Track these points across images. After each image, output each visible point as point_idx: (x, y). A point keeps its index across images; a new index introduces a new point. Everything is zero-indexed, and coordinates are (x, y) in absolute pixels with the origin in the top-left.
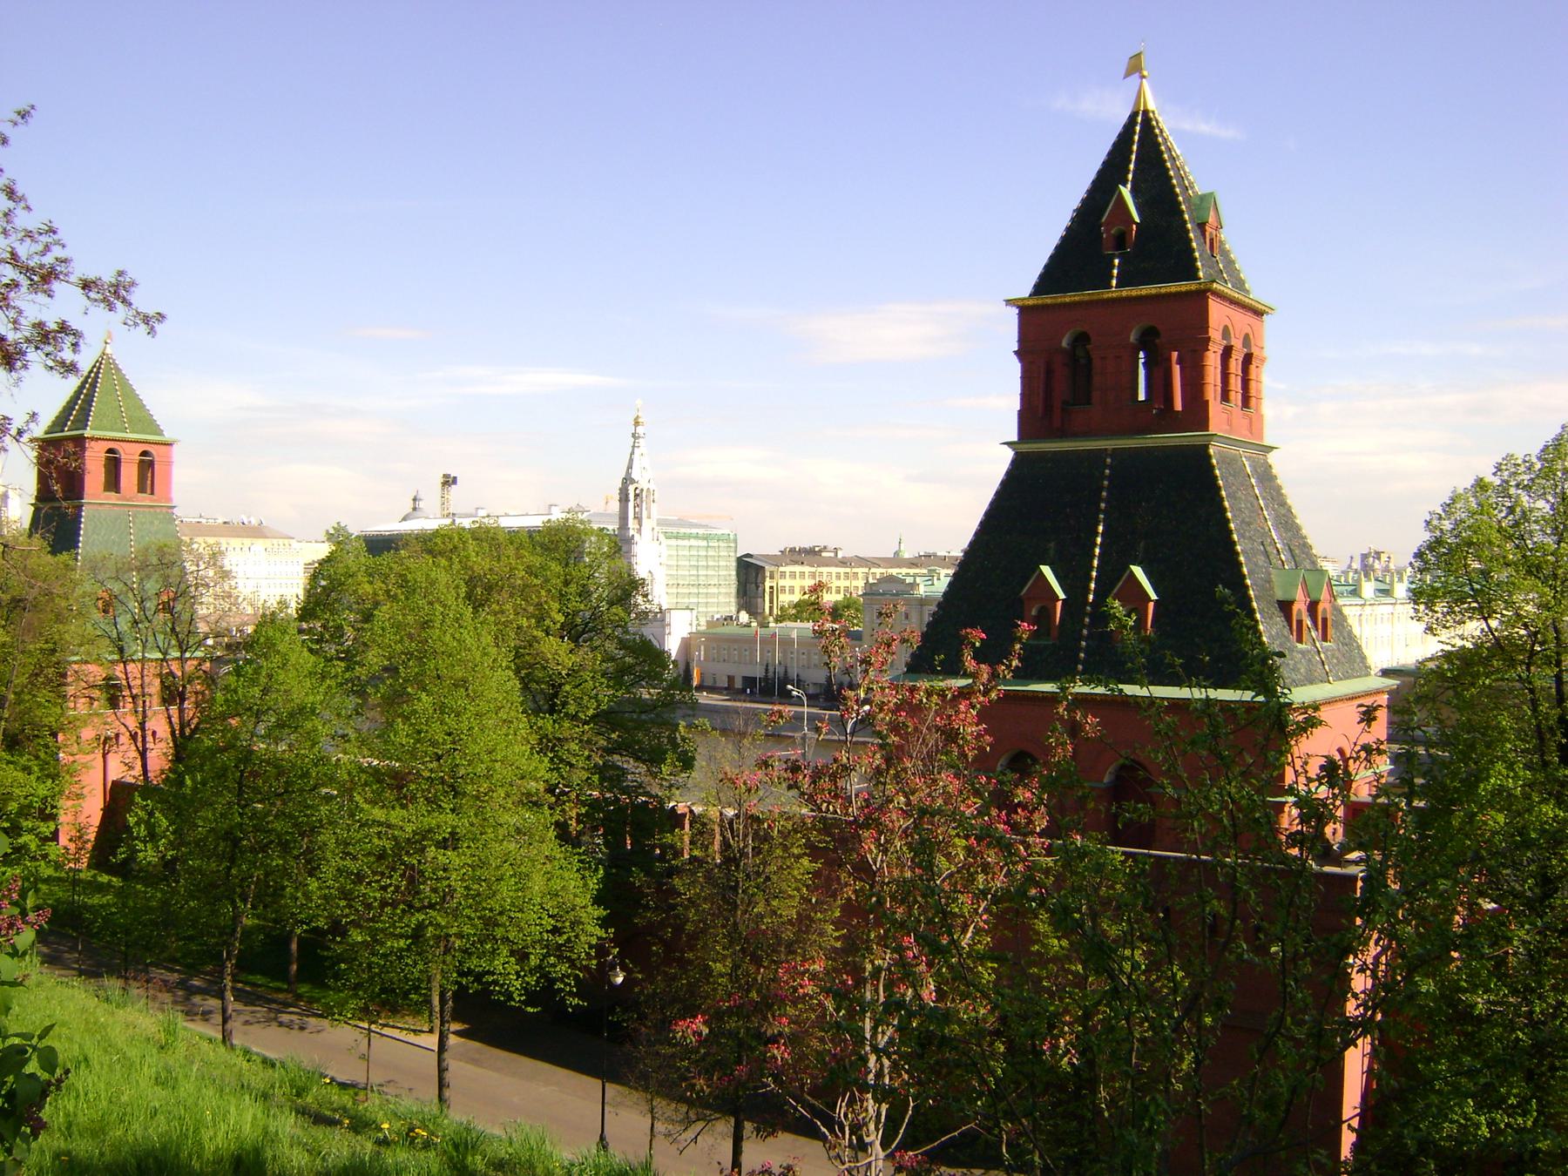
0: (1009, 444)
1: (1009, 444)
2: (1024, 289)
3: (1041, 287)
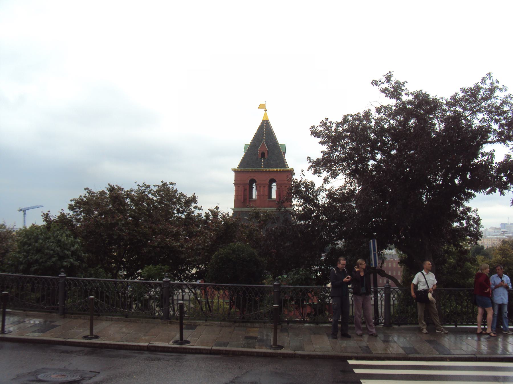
0: (232, 209)
1: (232, 209)
2: (236, 166)
3: (240, 166)
